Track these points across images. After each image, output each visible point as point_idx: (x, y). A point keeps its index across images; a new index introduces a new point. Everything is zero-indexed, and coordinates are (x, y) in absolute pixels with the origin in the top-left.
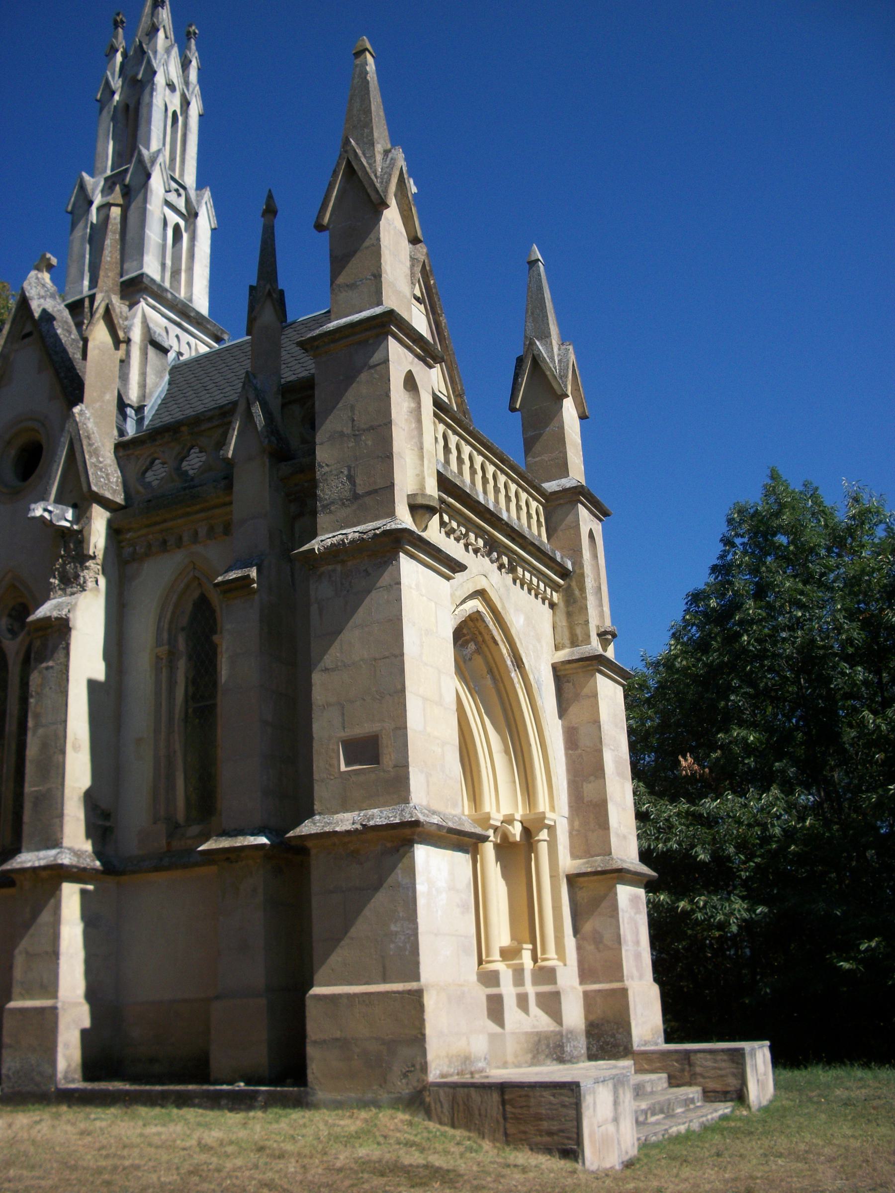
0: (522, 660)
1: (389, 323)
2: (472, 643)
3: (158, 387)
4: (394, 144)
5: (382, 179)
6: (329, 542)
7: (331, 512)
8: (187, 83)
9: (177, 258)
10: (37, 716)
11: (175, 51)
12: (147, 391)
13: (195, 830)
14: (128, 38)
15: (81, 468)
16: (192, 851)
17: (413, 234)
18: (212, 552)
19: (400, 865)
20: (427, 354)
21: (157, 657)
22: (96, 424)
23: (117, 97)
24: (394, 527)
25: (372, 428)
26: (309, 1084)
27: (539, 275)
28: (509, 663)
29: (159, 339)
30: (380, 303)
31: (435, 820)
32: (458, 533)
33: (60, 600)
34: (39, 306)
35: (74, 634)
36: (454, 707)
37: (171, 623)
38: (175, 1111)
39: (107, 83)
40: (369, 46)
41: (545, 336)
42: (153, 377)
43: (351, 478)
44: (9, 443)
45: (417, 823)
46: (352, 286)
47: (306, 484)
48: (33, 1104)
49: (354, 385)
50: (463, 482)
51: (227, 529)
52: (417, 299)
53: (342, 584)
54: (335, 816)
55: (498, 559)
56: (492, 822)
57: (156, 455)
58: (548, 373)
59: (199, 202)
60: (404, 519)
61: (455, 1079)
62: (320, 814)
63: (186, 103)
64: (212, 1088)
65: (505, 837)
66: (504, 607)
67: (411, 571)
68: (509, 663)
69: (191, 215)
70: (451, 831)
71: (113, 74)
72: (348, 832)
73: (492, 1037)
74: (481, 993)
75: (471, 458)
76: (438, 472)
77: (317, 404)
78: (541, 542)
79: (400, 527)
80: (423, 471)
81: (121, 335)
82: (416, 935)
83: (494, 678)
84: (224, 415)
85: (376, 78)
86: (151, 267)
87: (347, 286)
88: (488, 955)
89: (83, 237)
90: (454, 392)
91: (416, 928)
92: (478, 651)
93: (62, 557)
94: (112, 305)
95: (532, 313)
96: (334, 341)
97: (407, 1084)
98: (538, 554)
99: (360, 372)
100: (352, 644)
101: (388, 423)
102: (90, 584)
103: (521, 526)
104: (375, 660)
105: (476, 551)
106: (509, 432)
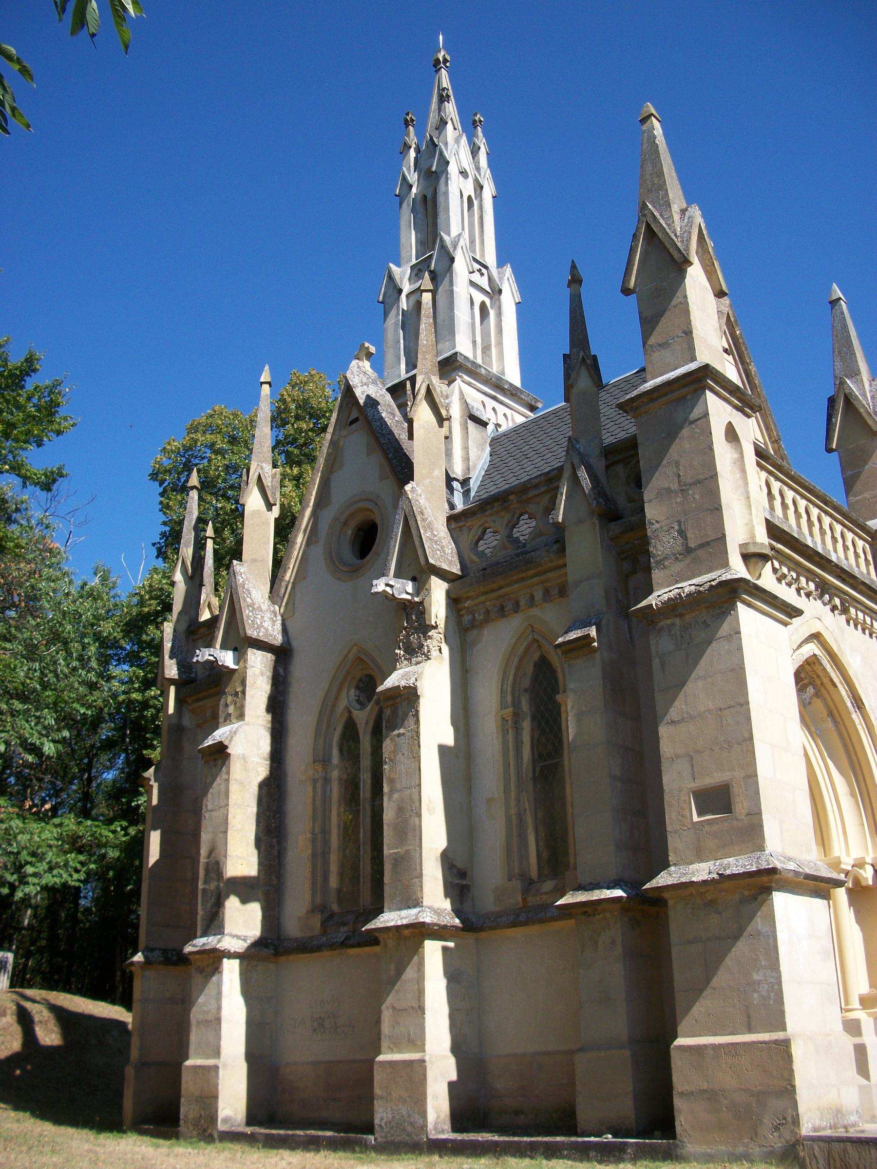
0: (861, 700)
1: (703, 378)
2: (811, 687)
3: (481, 459)
4: (689, 203)
5: (682, 238)
6: (665, 597)
7: (665, 567)
8: (478, 169)
9: (486, 335)
10: (392, 781)
11: (464, 139)
12: (471, 464)
13: (549, 885)
14: (420, 134)
15: (417, 543)
16: (547, 906)
17: (718, 288)
18: (549, 615)
19: (759, 914)
20: (745, 402)
21: (503, 719)
22: (429, 501)
23: (414, 190)
24: (729, 577)
25: (699, 482)
26: (678, 1136)
27: (842, 313)
28: (849, 704)
29: (477, 414)
30: (693, 359)
31: (792, 866)
32: (789, 578)
33: (406, 670)
34: (363, 393)
35: (421, 700)
36: (802, 753)
37: (514, 683)
38: (544, 1162)
39: (404, 178)
40: (654, 112)
41: (855, 373)
42: (475, 450)
43: (682, 533)
44: (345, 524)
45: (774, 871)
46: (664, 345)
47: (636, 542)
48: (406, 1154)
49: (677, 441)
50: (790, 526)
51: (563, 591)
52: (726, 351)
53: (682, 637)
54: (691, 867)
55: (830, 601)
56: (843, 866)
57: (487, 525)
58: (862, 410)
59: (501, 279)
60: (738, 569)
61: (828, 1133)
62: (675, 865)
63: (479, 187)
64: (580, 1139)
65: (857, 881)
66: (840, 649)
67: (749, 619)
68: (849, 704)
69: (495, 292)
70: (808, 877)
71: (409, 169)
72: (705, 882)
73: (861, 1087)
74: (848, 1042)
75: (794, 503)
76: (766, 519)
77: (642, 463)
78: (871, 579)
79: (735, 577)
80: (751, 520)
81: (444, 413)
82: (780, 983)
83: (835, 722)
84: (550, 481)
85: (664, 141)
86: (463, 346)
87: (660, 345)
88: (847, 1003)
89: (396, 324)
90: (770, 438)
91: (780, 976)
92: (817, 694)
93: (405, 628)
94: (433, 385)
95: (840, 352)
96: (653, 400)
97: (780, 1137)
98: (869, 592)
99: (681, 428)
100: (697, 695)
101: (714, 476)
102: (434, 653)
103: (850, 566)
104: (721, 709)
105: (808, 595)
106: (828, 473)
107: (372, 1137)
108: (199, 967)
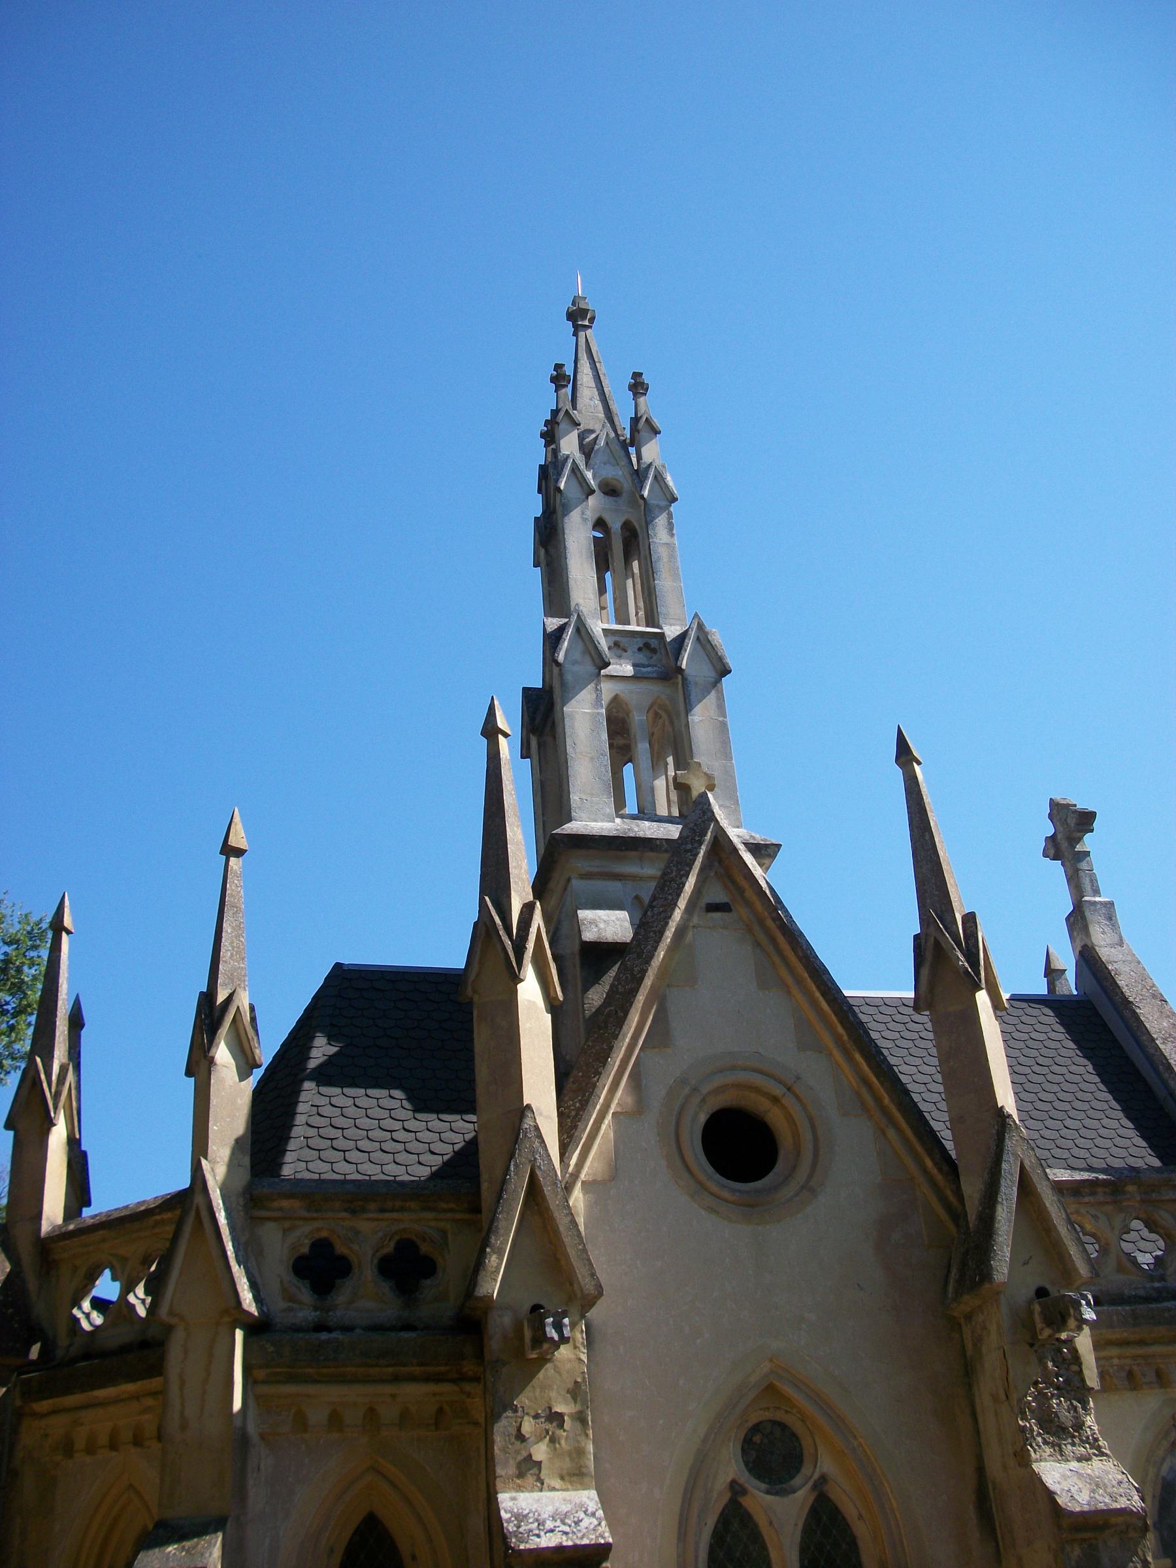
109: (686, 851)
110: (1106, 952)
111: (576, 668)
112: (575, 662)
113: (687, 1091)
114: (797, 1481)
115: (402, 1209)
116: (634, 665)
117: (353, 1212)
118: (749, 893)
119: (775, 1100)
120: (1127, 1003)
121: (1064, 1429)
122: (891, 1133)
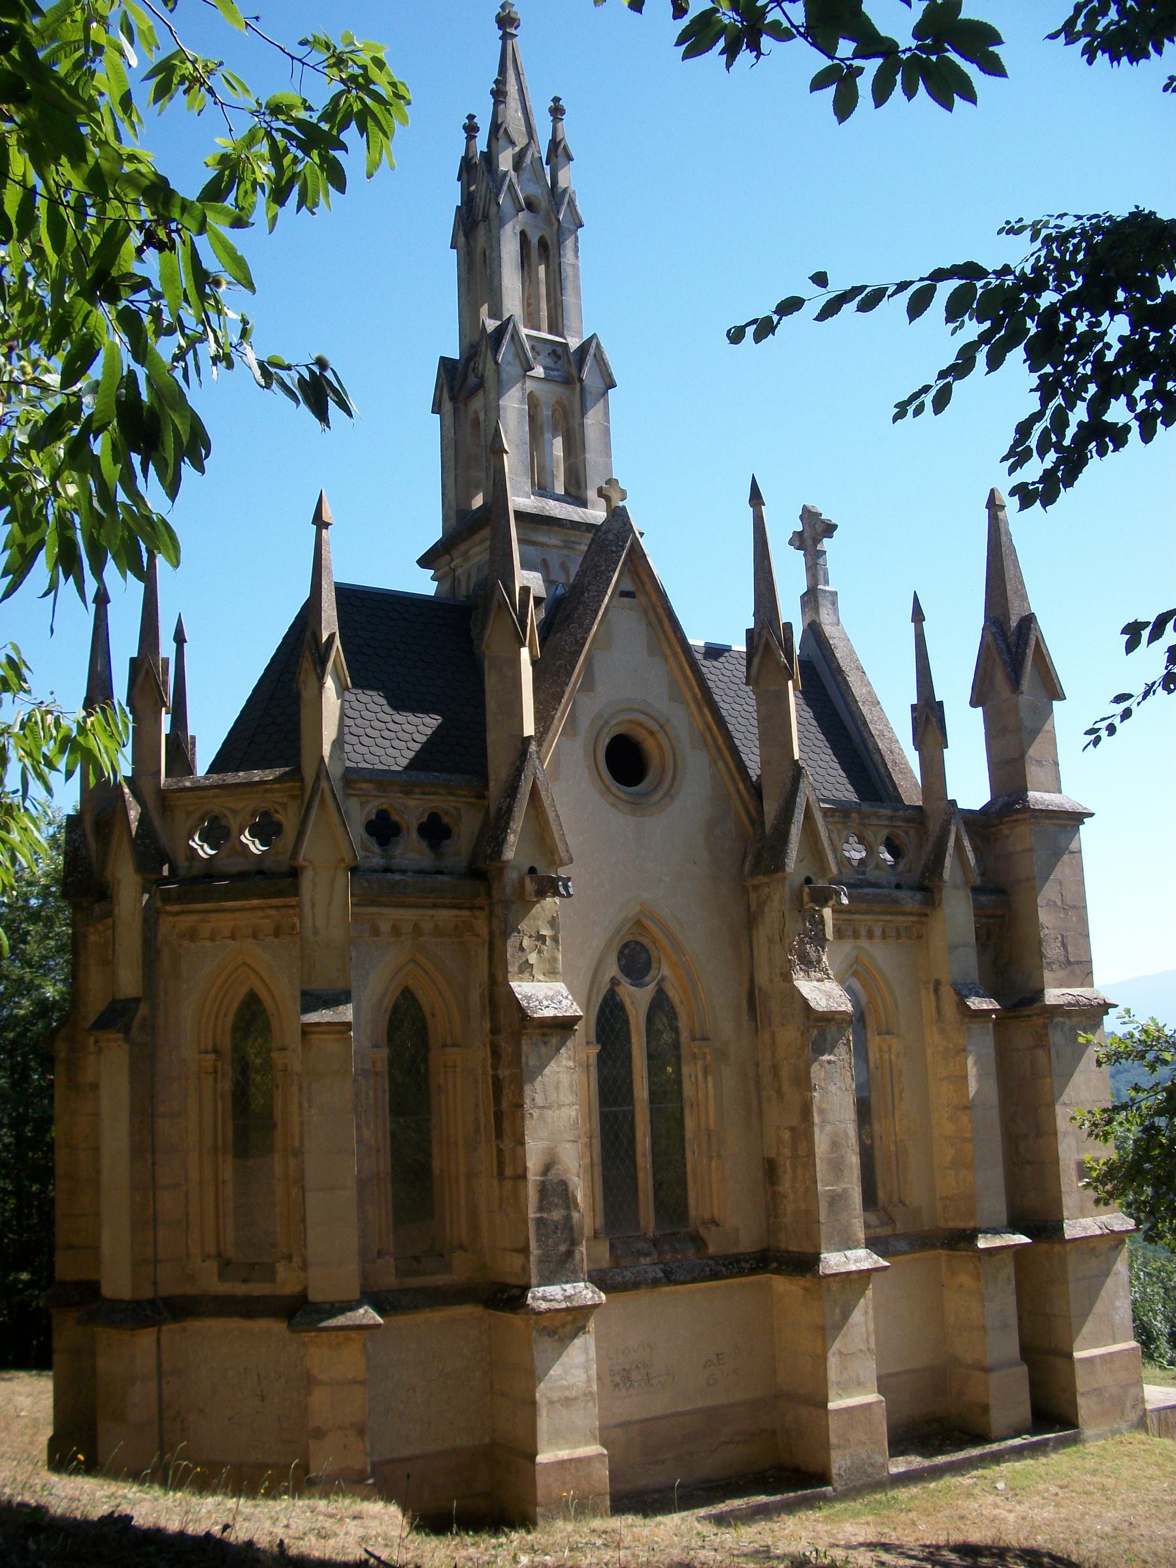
107: (830, 1488)
108: (545, 1328)
109: (612, 552)
110: (828, 630)
111: (508, 369)
112: (509, 364)
113: (602, 722)
114: (647, 979)
115: (434, 794)
116: (545, 368)
117: (406, 793)
118: (649, 587)
119: (652, 733)
120: (840, 670)
121: (811, 962)
122: (721, 764)
